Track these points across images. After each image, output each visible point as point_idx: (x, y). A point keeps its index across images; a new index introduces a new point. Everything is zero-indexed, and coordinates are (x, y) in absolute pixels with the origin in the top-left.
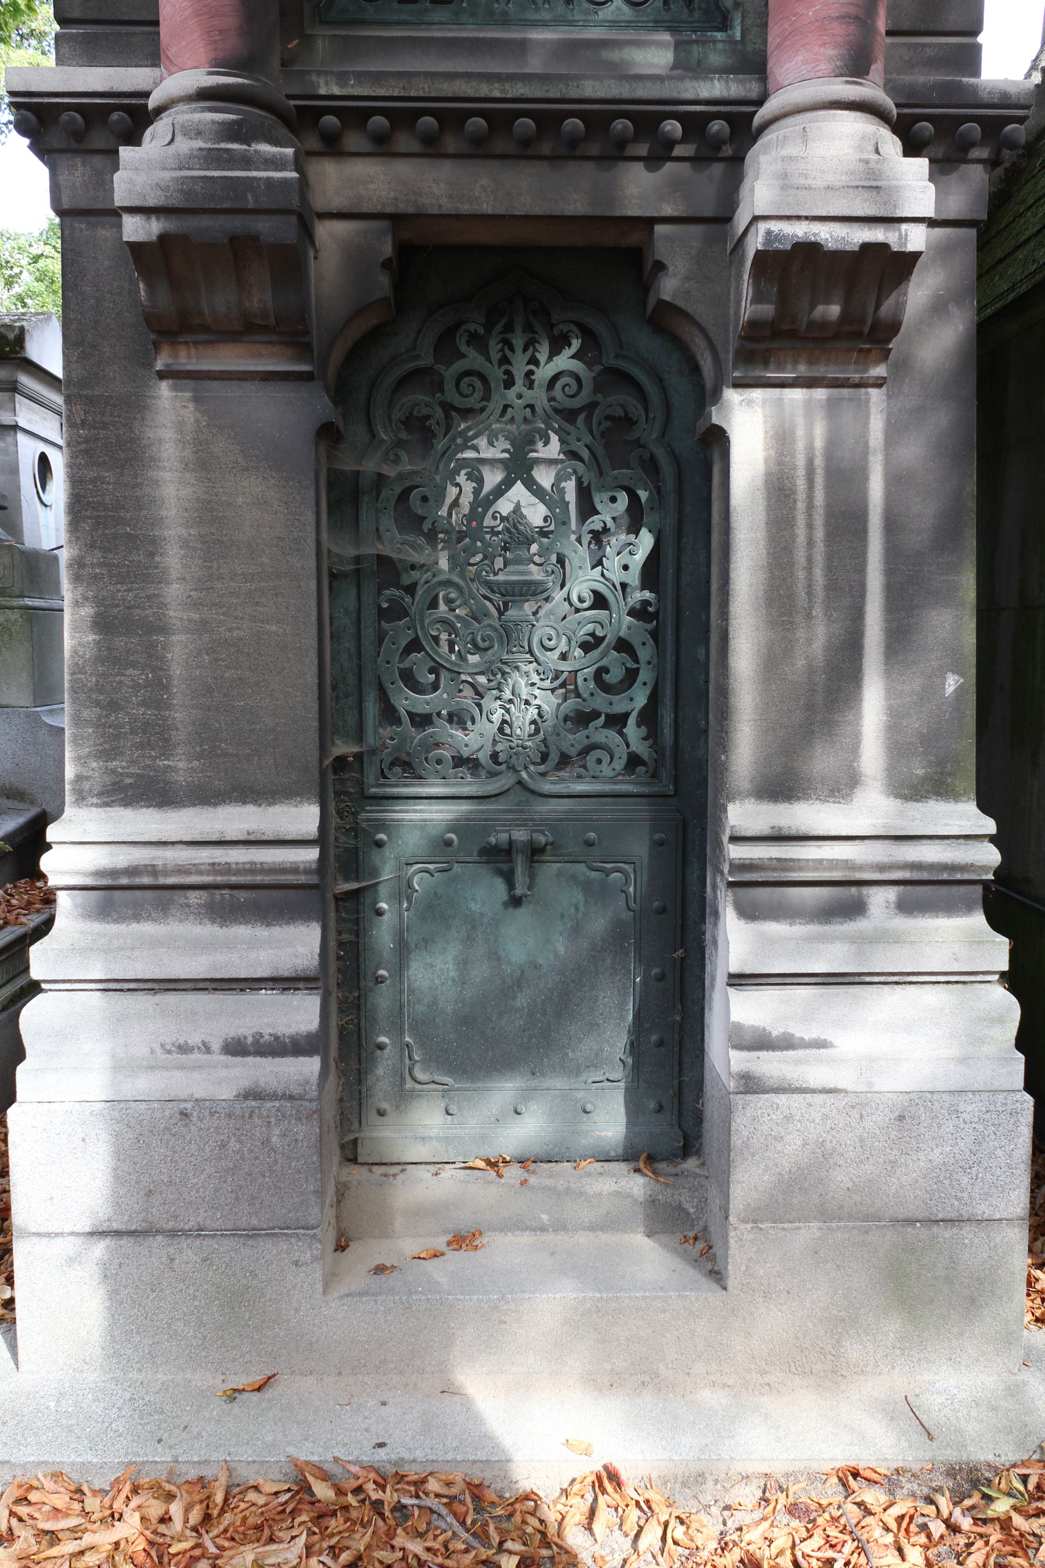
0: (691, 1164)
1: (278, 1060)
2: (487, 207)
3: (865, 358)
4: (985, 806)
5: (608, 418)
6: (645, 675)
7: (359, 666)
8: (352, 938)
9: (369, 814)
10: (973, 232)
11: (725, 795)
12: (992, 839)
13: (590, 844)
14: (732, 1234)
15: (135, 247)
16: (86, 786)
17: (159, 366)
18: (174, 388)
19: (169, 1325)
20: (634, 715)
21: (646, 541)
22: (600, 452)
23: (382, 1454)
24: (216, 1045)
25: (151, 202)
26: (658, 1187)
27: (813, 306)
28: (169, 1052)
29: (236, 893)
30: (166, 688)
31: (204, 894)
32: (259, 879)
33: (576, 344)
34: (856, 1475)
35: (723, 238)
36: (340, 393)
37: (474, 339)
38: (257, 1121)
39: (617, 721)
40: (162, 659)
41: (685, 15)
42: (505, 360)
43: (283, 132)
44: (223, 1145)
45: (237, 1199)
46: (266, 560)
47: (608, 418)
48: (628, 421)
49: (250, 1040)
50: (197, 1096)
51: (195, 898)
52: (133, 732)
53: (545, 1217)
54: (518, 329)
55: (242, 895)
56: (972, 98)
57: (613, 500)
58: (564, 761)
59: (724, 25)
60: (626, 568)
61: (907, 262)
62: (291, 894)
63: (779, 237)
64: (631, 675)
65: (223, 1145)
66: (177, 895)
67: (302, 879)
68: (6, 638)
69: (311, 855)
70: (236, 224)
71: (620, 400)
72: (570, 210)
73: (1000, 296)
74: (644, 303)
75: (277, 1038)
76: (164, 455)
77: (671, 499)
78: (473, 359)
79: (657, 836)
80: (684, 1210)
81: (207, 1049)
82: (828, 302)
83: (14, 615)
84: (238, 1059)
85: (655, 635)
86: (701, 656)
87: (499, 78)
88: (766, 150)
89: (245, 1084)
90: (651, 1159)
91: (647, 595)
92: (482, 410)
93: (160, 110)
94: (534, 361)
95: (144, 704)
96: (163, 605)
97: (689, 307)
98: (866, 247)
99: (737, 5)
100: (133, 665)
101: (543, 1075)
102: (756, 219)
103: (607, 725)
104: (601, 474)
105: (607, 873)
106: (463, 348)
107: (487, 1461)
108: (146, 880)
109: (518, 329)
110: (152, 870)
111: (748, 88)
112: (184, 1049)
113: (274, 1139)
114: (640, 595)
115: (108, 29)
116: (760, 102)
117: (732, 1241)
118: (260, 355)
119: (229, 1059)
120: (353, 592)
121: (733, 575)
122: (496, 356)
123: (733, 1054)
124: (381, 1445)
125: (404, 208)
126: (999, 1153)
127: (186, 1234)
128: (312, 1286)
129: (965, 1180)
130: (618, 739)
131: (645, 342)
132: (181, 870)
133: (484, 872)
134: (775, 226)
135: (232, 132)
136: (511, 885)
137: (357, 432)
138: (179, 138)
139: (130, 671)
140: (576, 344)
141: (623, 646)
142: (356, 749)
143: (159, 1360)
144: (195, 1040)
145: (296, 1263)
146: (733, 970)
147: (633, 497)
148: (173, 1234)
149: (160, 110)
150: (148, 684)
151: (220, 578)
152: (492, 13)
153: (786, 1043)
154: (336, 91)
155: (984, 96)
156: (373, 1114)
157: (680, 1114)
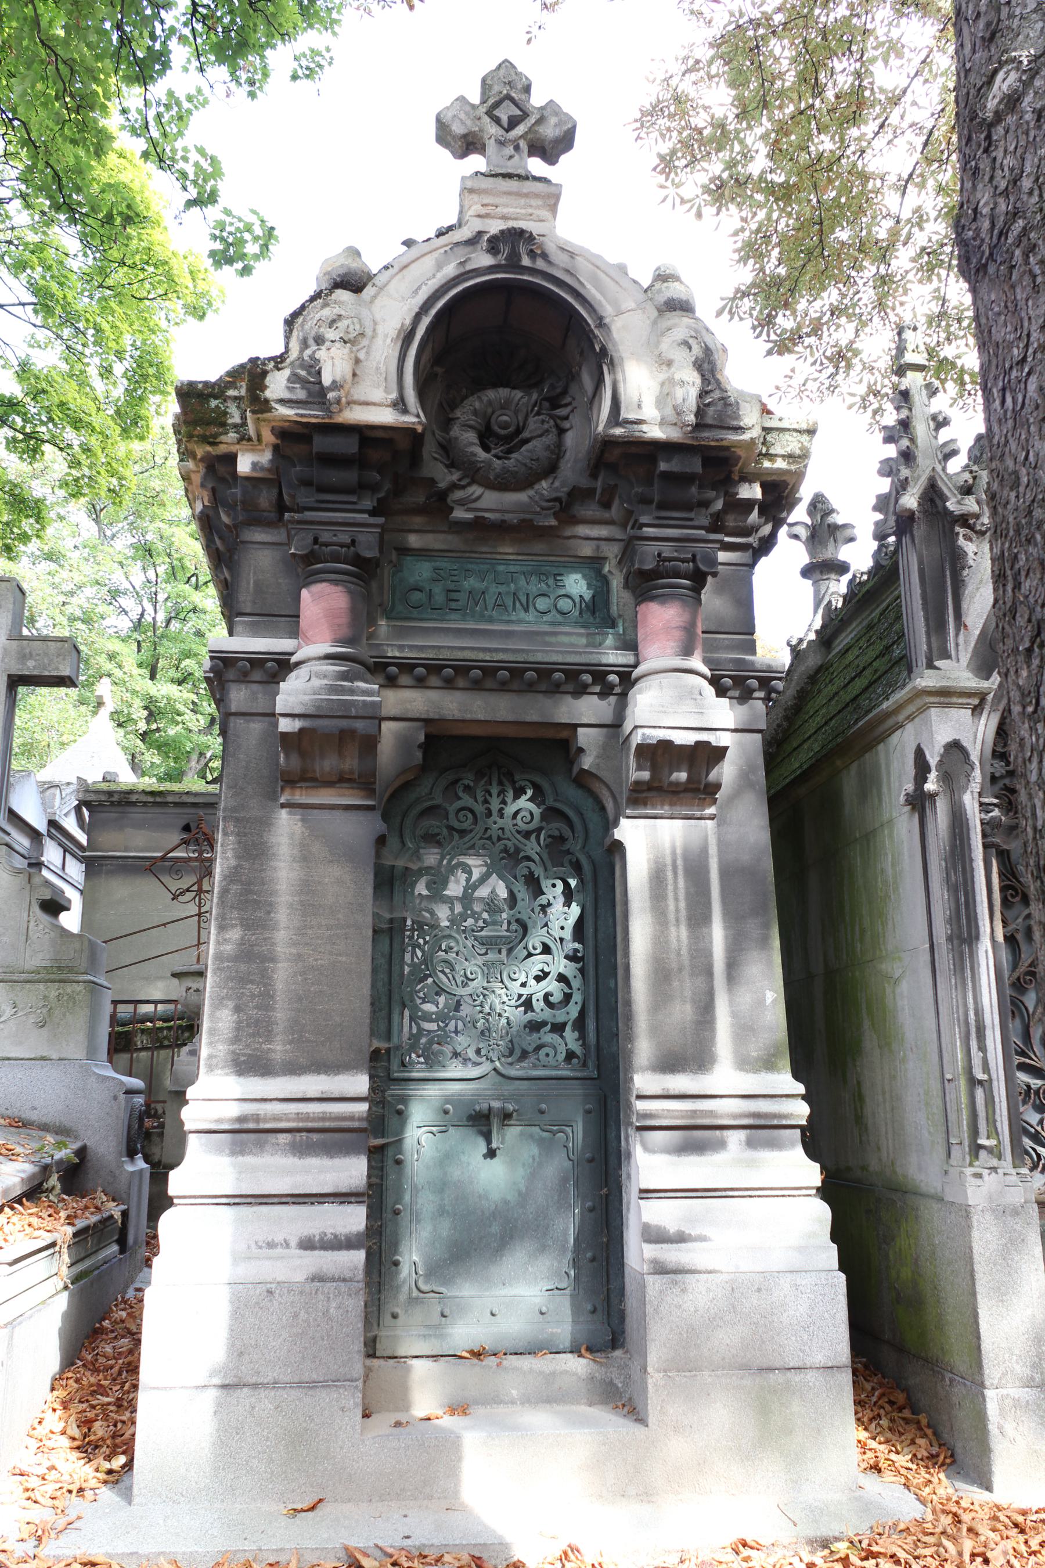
0: (618, 1353)
1: (336, 1253)
2: (481, 717)
3: (703, 806)
4: (797, 1076)
5: (550, 836)
6: (577, 997)
7: (390, 991)
8: (378, 1181)
9: (395, 1091)
10: (759, 736)
11: (629, 1069)
12: (804, 1097)
13: (542, 1112)
14: (650, 1381)
15: (284, 735)
16: (214, 1061)
17: (282, 800)
18: (290, 813)
19: (247, 1462)
20: (570, 1024)
21: (575, 910)
22: (545, 856)
23: (408, 1542)
24: (293, 1243)
25: (296, 712)
26: (596, 1367)
27: (671, 774)
28: (261, 1247)
29: (310, 1135)
30: (272, 997)
31: (288, 1136)
32: (327, 1124)
33: (530, 793)
34: (745, 1545)
35: (617, 736)
36: (386, 817)
37: (467, 789)
38: (321, 1297)
39: (559, 1028)
40: (270, 978)
41: (591, 620)
42: (486, 802)
43: (369, 676)
44: (296, 1316)
45: (303, 1358)
46: (340, 916)
47: (550, 836)
48: (562, 839)
49: (317, 1238)
50: (279, 1279)
51: (283, 1138)
52: (248, 1026)
53: (514, 1392)
54: (495, 783)
55: (315, 1137)
56: (750, 667)
57: (554, 886)
58: (524, 1055)
59: (613, 625)
60: (562, 928)
61: (719, 753)
62: (347, 1136)
63: (649, 737)
64: (567, 997)
65: (296, 1316)
66: (271, 1137)
67: (356, 1124)
68: (71, 1005)
69: (363, 1107)
70: (344, 723)
71: (556, 827)
72: (528, 719)
73: (794, 771)
74: (571, 770)
75: (336, 1236)
76: (281, 852)
77: (590, 886)
78: (467, 800)
79: (588, 1107)
80: (615, 1385)
81: (287, 1245)
82: (680, 771)
83: (79, 988)
84: (308, 1252)
85: (582, 971)
86: (612, 985)
87: (489, 650)
88: (640, 692)
89: (313, 1270)
90: (589, 1349)
91: (576, 945)
92: (471, 831)
93: (298, 664)
94: (504, 802)
95: (257, 1007)
96: (273, 944)
97: (599, 774)
98: (698, 744)
99: (620, 616)
100: (252, 982)
101: (511, 1285)
102: (636, 727)
103: (552, 1031)
104: (546, 870)
105: (554, 1133)
106: (461, 794)
107: (485, 1544)
108: (251, 1126)
109: (495, 783)
110: (257, 1118)
111: (630, 659)
112: (271, 1245)
113: (332, 1311)
114: (572, 946)
115: (266, 619)
116: (635, 666)
117: (650, 1387)
118: (344, 795)
119: (302, 1252)
120: (387, 941)
121: (631, 929)
122: (480, 799)
123: (645, 1246)
124: (408, 1537)
125: (432, 716)
126: (826, 1315)
127: (265, 1386)
128: (353, 1427)
129: (806, 1337)
130: (560, 1040)
131: (572, 792)
132: (277, 1119)
133: (470, 1133)
134: (647, 731)
135: (344, 676)
136: (489, 1142)
137: (393, 842)
138: (313, 679)
139: (250, 986)
140: (530, 793)
141: (562, 978)
142: (387, 1045)
143: (237, 1492)
144: (279, 1238)
145: (342, 1409)
146: (643, 1186)
147: (567, 885)
148: (255, 1386)
149: (298, 664)
150: (260, 995)
151: (311, 927)
152: (483, 616)
153: (681, 1238)
154: (398, 654)
155: (758, 666)
156: (388, 1317)
157: (609, 1315)
